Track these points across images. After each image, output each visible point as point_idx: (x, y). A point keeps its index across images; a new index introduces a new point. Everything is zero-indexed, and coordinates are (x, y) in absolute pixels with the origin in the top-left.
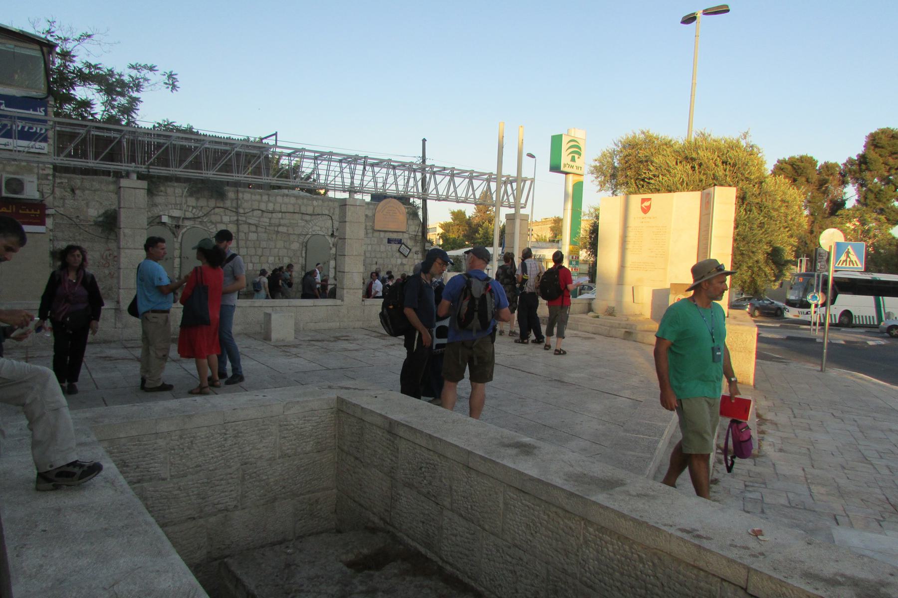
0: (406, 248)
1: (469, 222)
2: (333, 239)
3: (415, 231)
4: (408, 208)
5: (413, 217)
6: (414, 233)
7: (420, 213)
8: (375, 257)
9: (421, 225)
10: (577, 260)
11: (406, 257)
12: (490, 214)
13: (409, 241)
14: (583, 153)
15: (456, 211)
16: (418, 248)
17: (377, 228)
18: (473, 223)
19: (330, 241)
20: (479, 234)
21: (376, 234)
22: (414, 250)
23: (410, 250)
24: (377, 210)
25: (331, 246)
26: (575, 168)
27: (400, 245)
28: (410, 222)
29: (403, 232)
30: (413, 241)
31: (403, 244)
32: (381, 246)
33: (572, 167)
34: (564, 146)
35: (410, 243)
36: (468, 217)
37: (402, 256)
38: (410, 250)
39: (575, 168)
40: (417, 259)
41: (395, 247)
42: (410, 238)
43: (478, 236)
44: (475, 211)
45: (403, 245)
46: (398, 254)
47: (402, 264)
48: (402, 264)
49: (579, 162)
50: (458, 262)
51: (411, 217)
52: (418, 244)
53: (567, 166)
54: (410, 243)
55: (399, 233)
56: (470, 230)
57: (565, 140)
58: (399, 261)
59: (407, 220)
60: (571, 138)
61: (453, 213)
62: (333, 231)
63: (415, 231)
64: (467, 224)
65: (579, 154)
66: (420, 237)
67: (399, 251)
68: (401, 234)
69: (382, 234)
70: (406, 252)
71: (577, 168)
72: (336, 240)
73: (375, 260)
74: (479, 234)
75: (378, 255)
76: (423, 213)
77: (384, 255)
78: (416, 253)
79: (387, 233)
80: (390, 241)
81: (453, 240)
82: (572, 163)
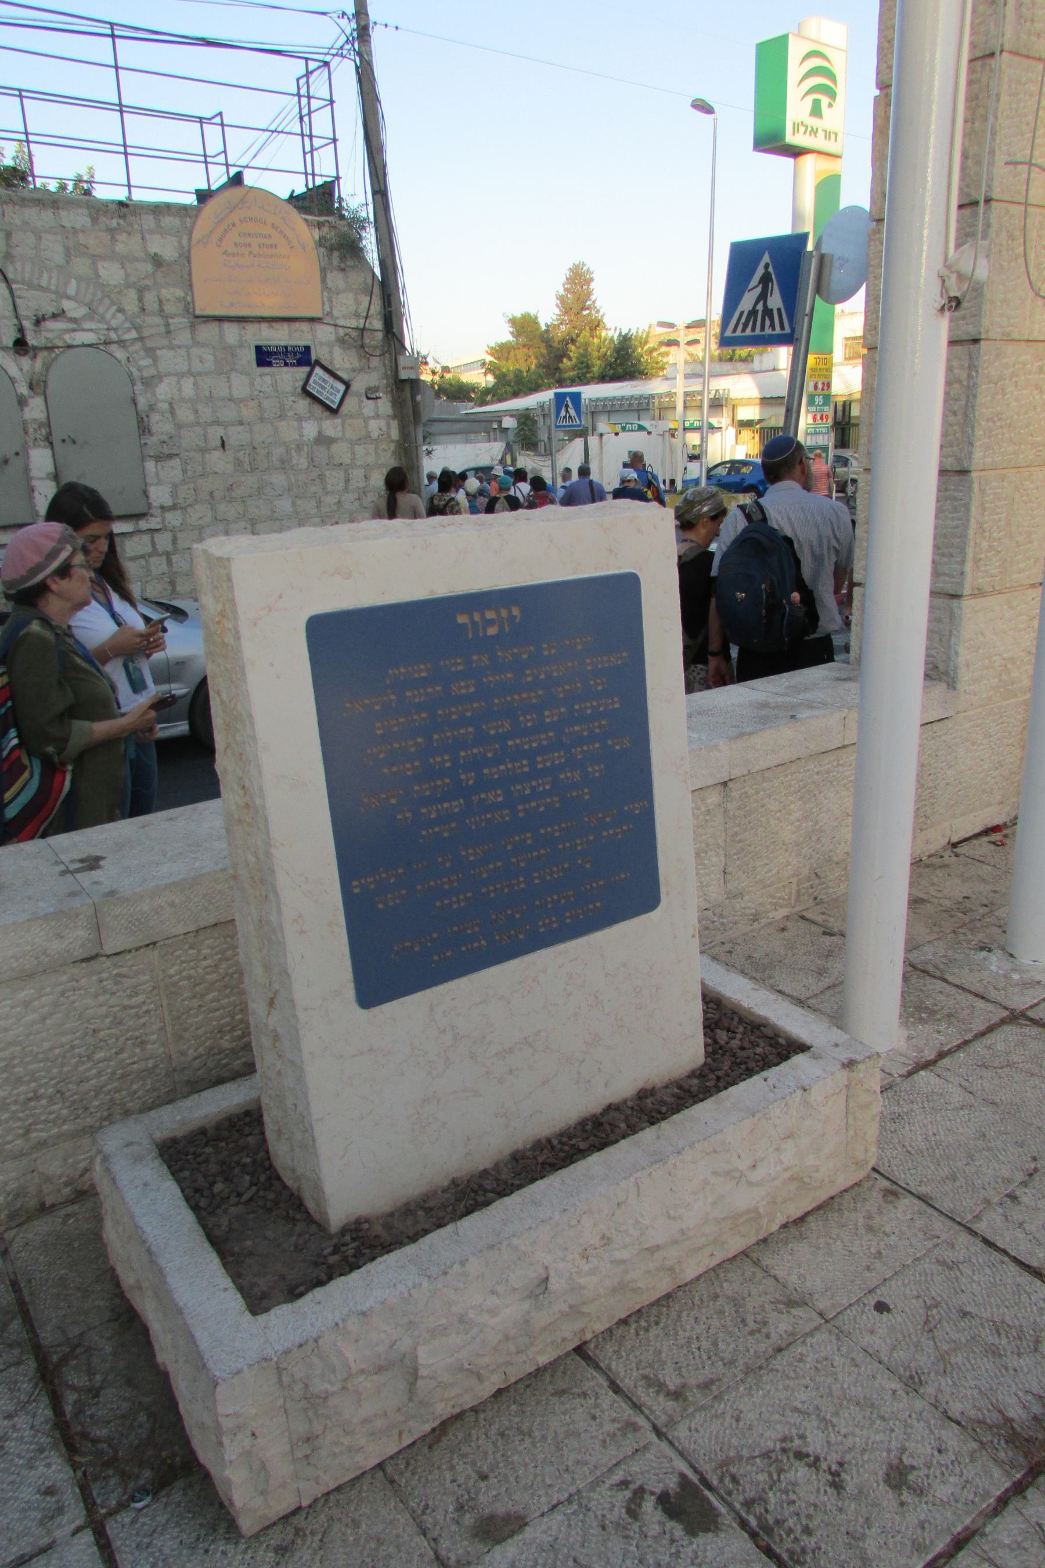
0: (331, 380)
1: (545, 338)
2: (25, 362)
3: (357, 315)
4: (320, 225)
5: (342, 259)
6: (353, 323)
7: (369, 241)
8: (217, 423)
9: (377, 290)
10: (825, 392)
11: (334, 412)
12: (588, 315)
13: (338, 351)
14: (840, 90)
15: (519, 316)
16: (374, 377)
17: (205, 306)
18: (556, 340)
19: (14, 371)
20: (570, 359)
21: (208, 332)
22: (359, 384)
23: (347, 385)
24: (197, 235)
25: (24, 390)
26: (821, 134)
27: (307, 369)
28: (336, 279)
29: (312, 320)
30: (353, 353)
31: (318, 363)
32: (234, 376)
33: (814, 132)
34: (795, 70)
35: (343, 361)
36: (544, 328)
37: (318, 409)
38: (347, 385)
39: (821, 134)
40: (377, 416)
41: (290, 377)
42: (341, 341)
43: (569, 363)
44: (557, 311)
45: (318, 370)
46: (303, 405)
47: (322, 440)
48: (322, 440)
49: (833, 117)
50: (529, 423)
51: (336, 261)
52: (375, 362)
53: (802, 129)
54: (343, 361)
55: (297, 325)
56: (550, 353)
57: (796, 50)
58: (310, 430)
59: (323, 271)
60: (810, 47)
61: (513, 322)
62: (21, 330)
63: (357, 315)
64: (543, 341)
65: (832, 94)
66: (380, 335)
67: (306, 392)
68: (305, 326)
69: (231, 332)
70: (330, 391)
71: (827, 135)
72: (39, 363)
73: (219, 432)
74: (570, 359)
75: (228, 413)
76: (379, 242)
77: (248, 413)
78: (370, 395)
79: (251, 328)
80: (264, 357)
81: (517, 376)
82: (814, 122)
